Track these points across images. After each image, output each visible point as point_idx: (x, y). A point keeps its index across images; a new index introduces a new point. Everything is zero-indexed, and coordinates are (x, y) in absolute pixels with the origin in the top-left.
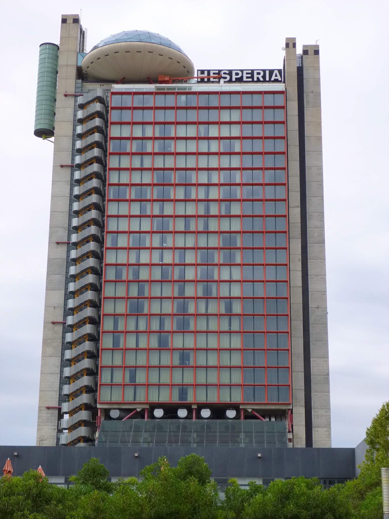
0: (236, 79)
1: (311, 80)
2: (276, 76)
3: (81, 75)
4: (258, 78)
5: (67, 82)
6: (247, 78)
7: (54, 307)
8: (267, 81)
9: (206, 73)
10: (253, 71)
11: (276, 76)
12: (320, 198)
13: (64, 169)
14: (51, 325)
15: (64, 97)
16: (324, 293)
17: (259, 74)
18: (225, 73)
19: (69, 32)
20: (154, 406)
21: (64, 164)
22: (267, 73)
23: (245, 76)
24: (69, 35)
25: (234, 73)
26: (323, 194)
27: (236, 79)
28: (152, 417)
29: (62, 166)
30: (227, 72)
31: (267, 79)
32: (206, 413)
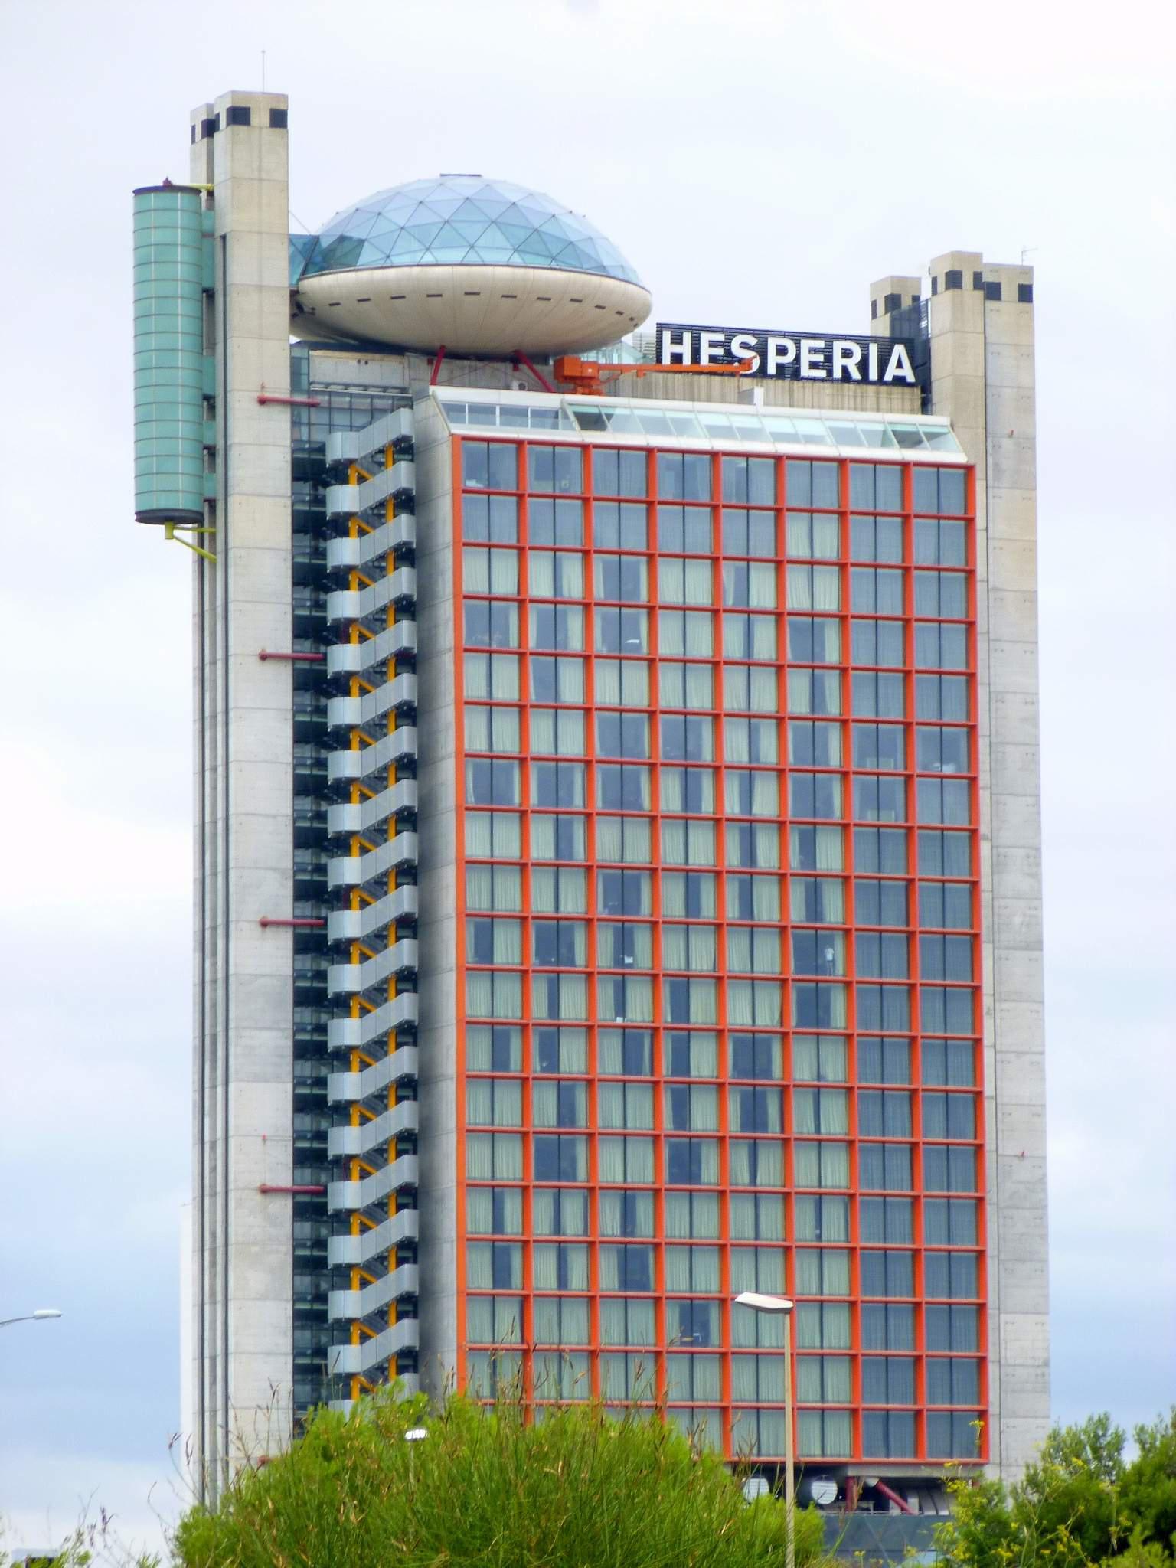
0: (780, 367)
1: (1008, 390)
2: (900, 365)
3: (316, 325)
4: (845, 369)
5: (261, 350)
6: (814, 365)
7: (264, 1138)
8: (873, 383)
9: (687, 337)
10: (830, 339)
11: (900, 365)
12: (1030, 800)
13: (270, 667)
14: (259, 1197)
16: (1038, 1110)
17: (847, 354)
18: (744, 346)
19: (260, 158)
21: (270, 650)
22: (873, 349)
23: (806, 358)
24: (260, 170)
25: (772, 343)
26: (1038, 787)
27: (780, 367)
29: (264, 657)
30: (753, 341)
31: (873, 375)
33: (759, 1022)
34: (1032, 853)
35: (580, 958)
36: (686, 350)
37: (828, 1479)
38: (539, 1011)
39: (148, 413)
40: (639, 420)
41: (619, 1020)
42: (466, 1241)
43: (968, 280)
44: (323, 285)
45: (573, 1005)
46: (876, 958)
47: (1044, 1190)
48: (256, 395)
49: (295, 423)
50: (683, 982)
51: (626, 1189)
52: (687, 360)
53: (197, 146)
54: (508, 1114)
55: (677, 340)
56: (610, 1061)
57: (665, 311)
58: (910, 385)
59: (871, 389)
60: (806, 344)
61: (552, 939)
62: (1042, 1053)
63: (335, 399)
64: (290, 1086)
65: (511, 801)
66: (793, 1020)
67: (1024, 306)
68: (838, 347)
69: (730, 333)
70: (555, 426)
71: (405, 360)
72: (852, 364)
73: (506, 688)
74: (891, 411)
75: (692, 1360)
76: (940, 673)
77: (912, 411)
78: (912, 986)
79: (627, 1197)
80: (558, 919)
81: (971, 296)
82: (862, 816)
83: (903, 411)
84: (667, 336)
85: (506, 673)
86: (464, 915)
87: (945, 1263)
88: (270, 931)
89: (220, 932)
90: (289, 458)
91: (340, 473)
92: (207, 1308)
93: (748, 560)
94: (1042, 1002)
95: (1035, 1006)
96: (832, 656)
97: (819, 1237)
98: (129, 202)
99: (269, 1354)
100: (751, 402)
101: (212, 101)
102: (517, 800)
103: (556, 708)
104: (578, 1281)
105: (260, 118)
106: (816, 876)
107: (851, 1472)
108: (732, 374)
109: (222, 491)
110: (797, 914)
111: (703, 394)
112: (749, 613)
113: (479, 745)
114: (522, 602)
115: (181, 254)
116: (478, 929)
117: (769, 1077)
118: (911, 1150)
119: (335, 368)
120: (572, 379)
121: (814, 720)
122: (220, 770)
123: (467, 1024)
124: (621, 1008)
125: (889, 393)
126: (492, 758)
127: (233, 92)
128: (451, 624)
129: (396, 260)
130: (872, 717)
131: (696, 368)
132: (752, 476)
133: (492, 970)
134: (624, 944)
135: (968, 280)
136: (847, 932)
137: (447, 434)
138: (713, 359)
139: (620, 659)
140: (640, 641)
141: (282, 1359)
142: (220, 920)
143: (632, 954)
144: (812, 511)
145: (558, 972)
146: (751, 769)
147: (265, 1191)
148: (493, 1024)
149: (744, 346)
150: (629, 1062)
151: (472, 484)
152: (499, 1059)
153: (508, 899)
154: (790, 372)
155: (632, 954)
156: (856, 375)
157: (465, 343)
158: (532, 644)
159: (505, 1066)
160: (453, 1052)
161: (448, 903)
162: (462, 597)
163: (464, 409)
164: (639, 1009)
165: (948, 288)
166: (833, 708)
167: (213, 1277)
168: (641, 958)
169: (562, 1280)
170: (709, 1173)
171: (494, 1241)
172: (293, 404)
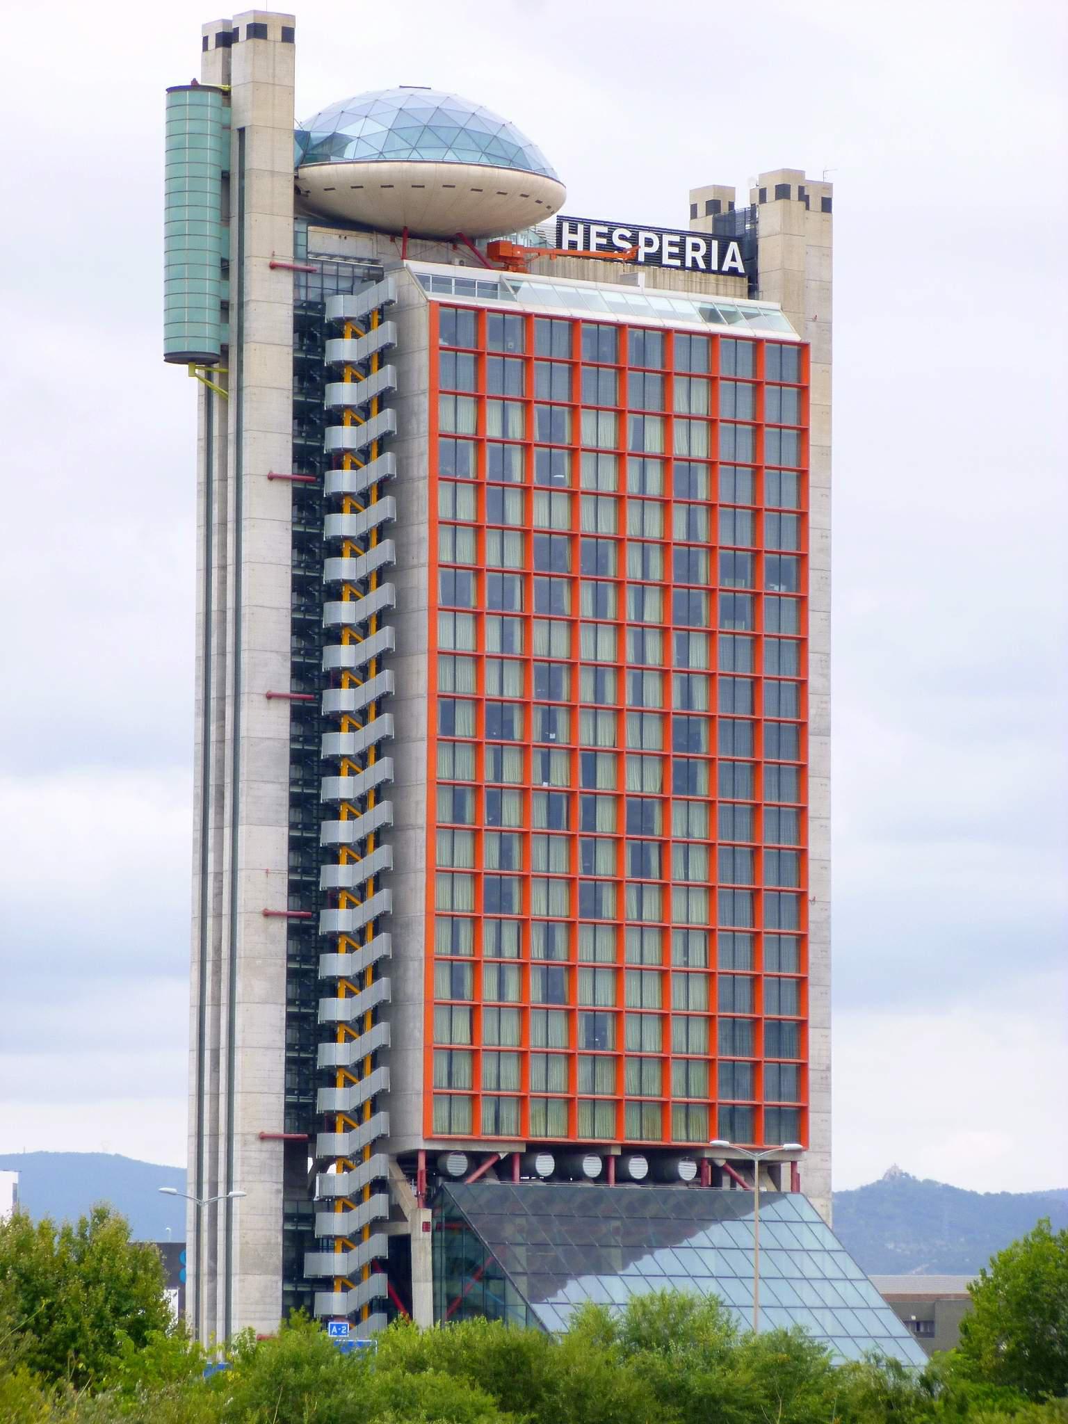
0: (647, 255)
2: (734, 259)
3: (312, 209)
4: (694, 260)
5: (271, 227)
6: (671, 256)
7: (267, 872)
8: (714, 272)
9: (581, 228)
11: (734, 259)
12: (823, 615)
13: (276, 485)
15: (268, 271)
18: (622, 237)
20: (536, 1148)
21: (276, 472)
23: (667, 249)
25: (642, 236)
27: (647, 255)
28: (530, 1171)
29: (271, 478)
30: (628, 234)
31: (715, 267)
32: (592, 1166)
33: (646, 789)
34: (824, 657)
35: (517, 734)
36: (579, 238)
37: (690, 1160)
38: (488, 776)
39: (177, 272)
40: (543, 294)
41: (545, 785)
42: (432, 960)
43: (794, 193)
44: (316, 172)
45: (512, 773)
46: (730, 738)
47: (829, 929)
48: (268, 261)
49: (297, 286)
50: (592, 755)
51: (548, 921)
52: (580, 247)
53: (210, 54)
54: (463, 859)
55: (573, 230)
56: (539, 819)
57: (567, 210)
58: (741, 275)
59: (713, 277)
60: (667, 238)
61: (493, 715)
62: (829, 818)
63: (325, 267)
64: (286, 830)
65: (467, 604)
66: (671, 785)
67: (825, 215)
68: (690, 241)
69: (612, 226)
70: (495, 297)
71: (374, 237)
72: (699, 255)
73: (466, 512)
74: (726, 295)
75: (594, 1061)
76: (780, 511)
77: (741, 296)
78: (758, 763)
79: (549, 926)
80: (502, 701)
81: (795, 204)
82: (722, 625)
83: (735, 296)
84: (566, 226)
85: (467, 498)
86: (434, 696)
87: (776, 986)
88: (273, 703)
89: (229, 702)
90: (291, 314)
91: (336, 330)
92: (208, 1010)
93: (644, 414)
94: (829, 778)
95: (825, 781)
96: (702, 495)
97: (687, 964)
98: (162, 99)
99: (267, 1048)
100: (635, 283)
101: (230, 18)
102: (473, 603)
103: (503, 529)
104: (512, 995)
105: (275, 34)
106: (688, 673)
107: (707, 1155)
108: (612, 260)
109: (235, 338)
110: (676, 703)
111: (591, 274)
112: (644, 456)
113: (445, 557)
114: (479, 442)
115: (210, 142)
116: (444, 706)
117: (652, 834)
118: (752, 895)
119: (325, 240)
120: (504, 258)
121: (689, 546)
122: (231, 570)
123: (435, 784)
124: (546, 777)
125: (726, 281)
126: (455, 568)
127: (255, 12)
128: (426, 458)
129: (388, 156)
130: (731, 545)
131: (586, 253)
132: (648, 346)
133: (454, 741)
134: (549, 724)
135: (794, 193)
136: (711, 718)
137: (423, 301)
138: (599, 246)
139: (550, 490)
140: (563, 476)
141: (278, 1052)
142: (229, 691)
143: (554, 731)
144: (690, 376)
145: (502, 745)
146: (643, 584)
147: (267, 914)
148: (454, 785)
149: (622, 237)
150: (552, 820)
151: (441, 342)
152: (458, 815)
153: (466, 682)
154: (654, 260)
155: (554, 731)
156: (702, 265)
157: (420, 228)
158: (487, 477)
159: (462, 821)
160: (423, 806)
161: (419, 684)
162: (435, 434)
163: (427, 281)
164: (559, 778)
165: (777, 198)
166: (703, 537)
167: (217, 983)
168: (561, 735)
169: (501, 995)
170: (608, 910)
171: (452, 960)
172: (295, 270)
